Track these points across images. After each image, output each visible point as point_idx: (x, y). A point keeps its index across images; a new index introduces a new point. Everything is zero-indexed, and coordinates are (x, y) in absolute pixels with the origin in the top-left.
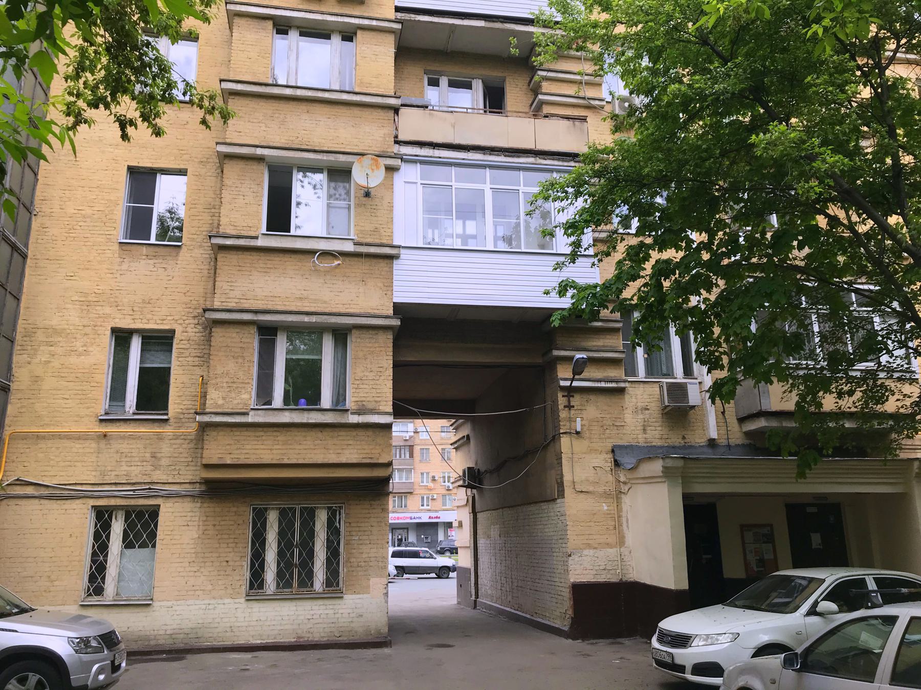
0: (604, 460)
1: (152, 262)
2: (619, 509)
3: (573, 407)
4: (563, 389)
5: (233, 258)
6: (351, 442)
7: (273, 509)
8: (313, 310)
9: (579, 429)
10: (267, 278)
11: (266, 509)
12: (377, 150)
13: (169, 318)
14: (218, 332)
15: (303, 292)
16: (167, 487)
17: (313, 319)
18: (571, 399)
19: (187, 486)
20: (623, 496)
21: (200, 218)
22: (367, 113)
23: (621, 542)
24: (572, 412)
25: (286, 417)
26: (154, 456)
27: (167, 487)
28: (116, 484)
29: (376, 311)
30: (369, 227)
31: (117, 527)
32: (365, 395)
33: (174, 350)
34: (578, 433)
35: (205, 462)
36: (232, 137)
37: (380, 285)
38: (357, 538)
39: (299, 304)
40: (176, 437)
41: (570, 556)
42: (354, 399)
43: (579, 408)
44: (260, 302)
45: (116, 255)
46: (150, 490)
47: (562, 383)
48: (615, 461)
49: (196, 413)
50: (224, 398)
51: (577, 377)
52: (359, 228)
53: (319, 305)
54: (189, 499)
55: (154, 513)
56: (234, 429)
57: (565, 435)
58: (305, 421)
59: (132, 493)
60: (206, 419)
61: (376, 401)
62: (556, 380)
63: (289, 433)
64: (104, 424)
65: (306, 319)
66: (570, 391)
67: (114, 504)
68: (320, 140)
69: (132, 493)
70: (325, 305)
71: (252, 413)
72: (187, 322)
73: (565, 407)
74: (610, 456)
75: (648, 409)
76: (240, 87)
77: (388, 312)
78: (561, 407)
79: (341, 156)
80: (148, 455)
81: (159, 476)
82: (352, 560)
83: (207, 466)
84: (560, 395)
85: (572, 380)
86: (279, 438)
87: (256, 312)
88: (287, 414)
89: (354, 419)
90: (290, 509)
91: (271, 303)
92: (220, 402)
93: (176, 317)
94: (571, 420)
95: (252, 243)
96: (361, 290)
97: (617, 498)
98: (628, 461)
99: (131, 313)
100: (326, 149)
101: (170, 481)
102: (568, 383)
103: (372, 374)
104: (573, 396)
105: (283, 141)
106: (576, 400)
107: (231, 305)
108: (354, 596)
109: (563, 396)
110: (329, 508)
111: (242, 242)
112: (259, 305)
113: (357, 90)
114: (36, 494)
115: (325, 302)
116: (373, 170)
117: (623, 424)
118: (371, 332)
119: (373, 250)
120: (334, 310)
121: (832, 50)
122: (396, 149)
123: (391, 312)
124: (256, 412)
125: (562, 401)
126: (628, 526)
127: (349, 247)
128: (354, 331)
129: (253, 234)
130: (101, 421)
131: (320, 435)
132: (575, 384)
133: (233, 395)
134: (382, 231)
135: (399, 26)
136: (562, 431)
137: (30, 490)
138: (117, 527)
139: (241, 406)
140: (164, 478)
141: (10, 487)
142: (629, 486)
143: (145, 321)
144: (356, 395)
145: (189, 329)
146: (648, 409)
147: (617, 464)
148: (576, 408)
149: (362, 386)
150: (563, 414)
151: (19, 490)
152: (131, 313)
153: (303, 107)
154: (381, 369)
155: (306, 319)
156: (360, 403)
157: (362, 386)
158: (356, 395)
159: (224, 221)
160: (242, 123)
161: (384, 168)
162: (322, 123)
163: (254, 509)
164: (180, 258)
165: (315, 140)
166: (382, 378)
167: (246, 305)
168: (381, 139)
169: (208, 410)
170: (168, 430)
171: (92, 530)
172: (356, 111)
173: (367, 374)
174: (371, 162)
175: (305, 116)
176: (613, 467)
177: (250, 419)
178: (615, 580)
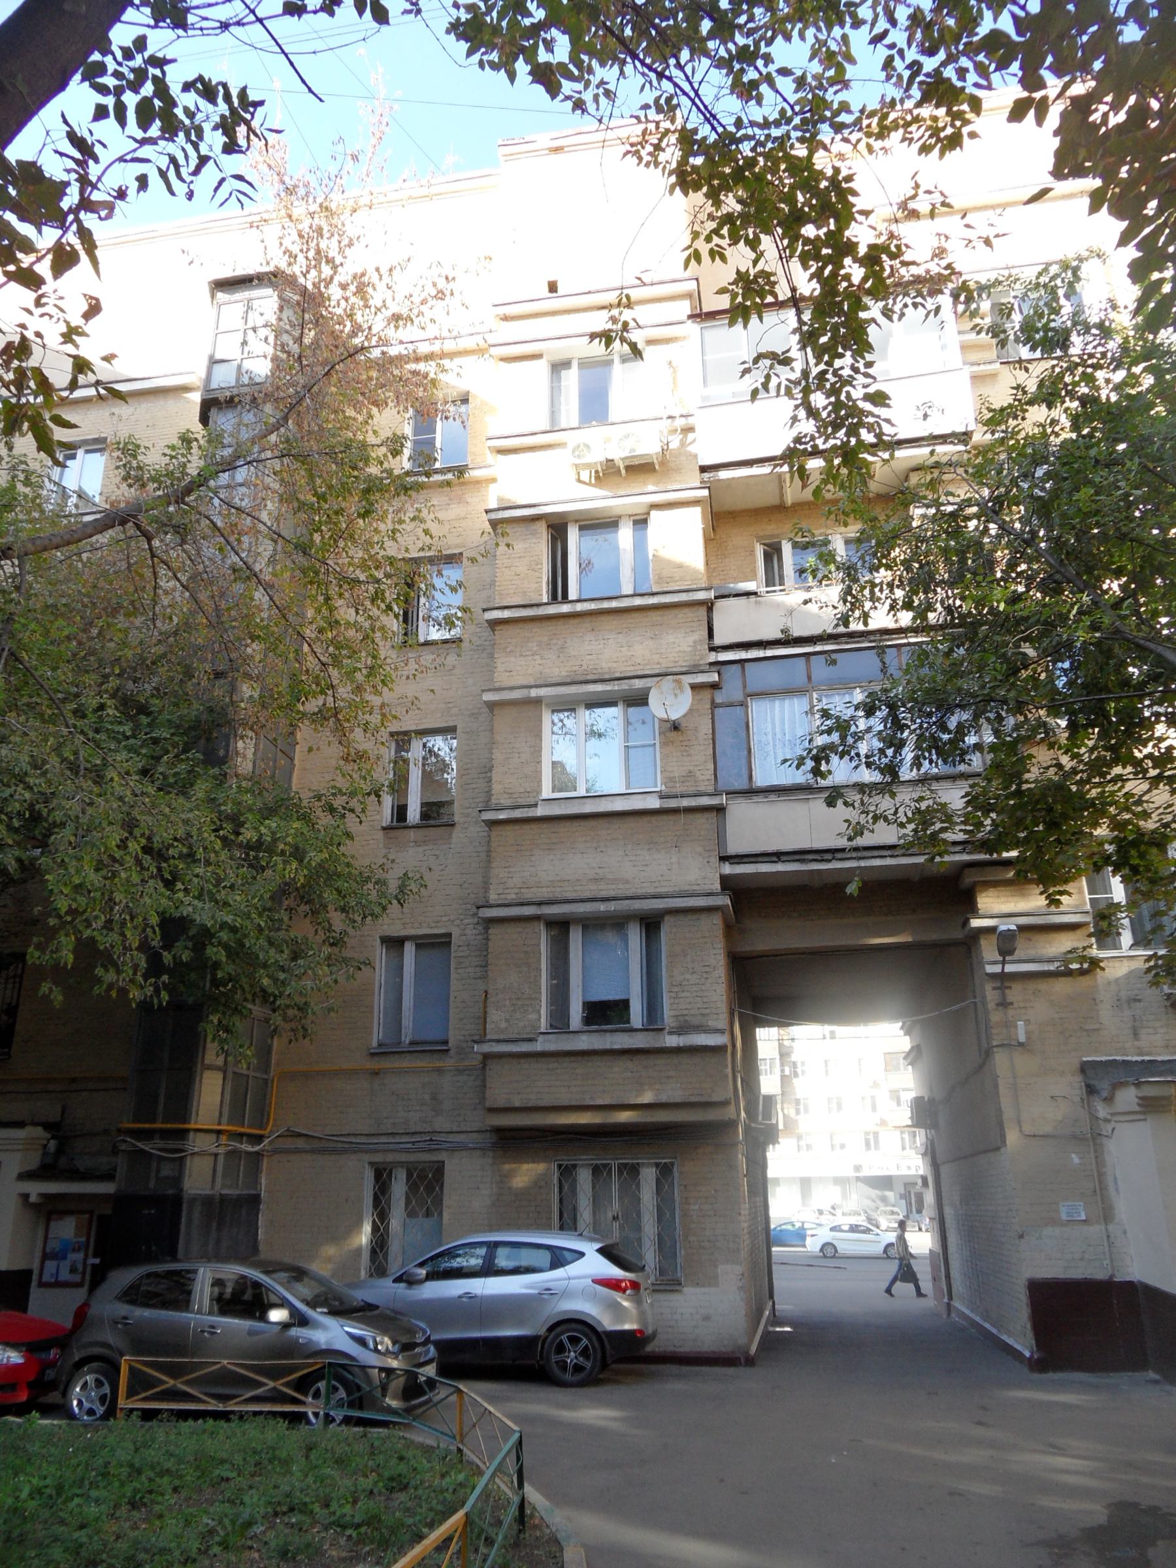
0: (1069, 1085)
1: (420, 849)
2: (1100, 1162)
3: (1012, 1004)
4: (993, 976)
5: (509, 832)
6: (672, 1073)
7: (582, 1165)
8: (612, 893)
9: (1022, 1039)
10: (551, 857)
11: (574, 1166)
12: (683, 665)
13: (444, 919)
14: (495, 932)
15: (598, 871)
16: (451, 1138)
17: (612, 906)
18: (1007, 991)
19: (475, 1135)
20: (1105, 1141)
21: (474, 786)
22: (669, 616)
23: (1107, 1215)
24: (1011, 1012)
25: (584, 1042)
26: (434, 1098)
27: (451, 1138)
28: (392, 1134)
29: (695, 887)
30: (678, 772)
31: (399, 1188)
32: (688, 1006)
33: (452, 960)
34: (1021, 1045)
35: (488, 1104)
36: (502, 678)
37: (699, 849)
38: (696, 1207)
39: (593, 887)
40: (460, 1071)
41: (1021, 1236)
42: (672, 1013)
43: (1021, 1005)
44: (544, 890)
45: (381, 845)
46: (432, 1140)
47: (990, 969)
48: (1088, 1086)
49: (475, 1042)
50: (507, 1021)
51: (1007, 958)
52: (667, 774)
53: (621, 886)
54: (478, 1153)
55: (439, 1169)
56: (522, 1061)
57: (1000, 1049)
58: (608, 1046)
59: (410, 1146)
60: (487, 1048)
61: (703, 1015)
62: (981, 964)
63: (590, 1064)
64: (376, 1058)
65: (603, 907)
66: (1004, 978)
67: (761, 1054)
68: (610, 665)
69: (410, 1146)
70: (627, 886)
71: (541, 1038)
72: (466, 921)
73: (998, 1005)
74: (1079, 1078)
75: (1139, 1001)
76: (506, 614)
77: (713, 887)
78: (991, 1006)
79: (637, 681)
80: (427, 1097)
81: (441, 1123)
82: (692, 1238)
83: (492, 1110)
84: (988, 987)
85: (1004, 963)
86: (578, 1071)
87: (540, 904)
88: (584, 1037)
89: (672, 1041)
90: (605, 1166)
91: (558, 889)
92: (503, 1025)
93: (452, 917)
94: (1009, 1025)
95: (531, 813)
96: (674, 860)
97: (1095, 1144)
98: (1104, 1086)
99: (400, 916)
100: (617, 675)
101: (455, 1129)
102: (997, 969)
103: (695, 976)
104: (1010, 988)
105: (564, 674)
106: (1015, 993)
107: (512, 897)
108: (698, 1290)
109: (994, 988)
110: (657, 1165)
111: (517, 814)
112: (544, 894)
113: (654, 590)
114: (307, 1147)
115: (627, 882)
116: (676, 695)
117: (1097, 1026)
118: (689, 917)
119: (685, 803)
120: (640, 892)
121: (868, 464)
122: (713, 657)
123: (717, 886)
124: (546, 1037)
125: (991, 994)
126: (1117, 1190)
127: (654, 803)
128: (667, 918)
129: (531, 801)
130: (373, 1054)
131: (629, 1064)
132: (1009, 968)
133: (518, 1015)
134: (698, 774)
135: (705, 493)
136: (995, 1043)
137: (300, 1143)
138: (399, 1188)
139: (528, 1029)
140: (447, 1126)
141: (281, 1139)
142: (1113, 1124)
143: (416, 925)
144: (675, 1007)
145: (468, 932)
146: (1139, 1001)
147: (1091, 1090)
148: (1016, 1005)
149: (683, 995)
150: (996, 1017)
151: (290, 1143)
152: (400, 916)
153: (587, 623)
154: (707, 969)
155: (603, 907)
156: (681, 1019)
157: (683, 995)
158: (675, 1007)
159: (496, 788)
160: (513, 659)
161: (689, 690)
162: (611, 641)
163: (560, 1166)
164: (454, 841)
165: (604, 665)
166: (709, 981)
167: (529, 895)
168: (690, 649)
169: (488, 1037)
170: (449, 1062)
171: (372, 1193)
172: (655, 616)
173: (688, 976)
174: (672, 685)
175: (590, 636)
176: (1085, 1096)
177: (538, 1046)
178: (1101, 1275)
